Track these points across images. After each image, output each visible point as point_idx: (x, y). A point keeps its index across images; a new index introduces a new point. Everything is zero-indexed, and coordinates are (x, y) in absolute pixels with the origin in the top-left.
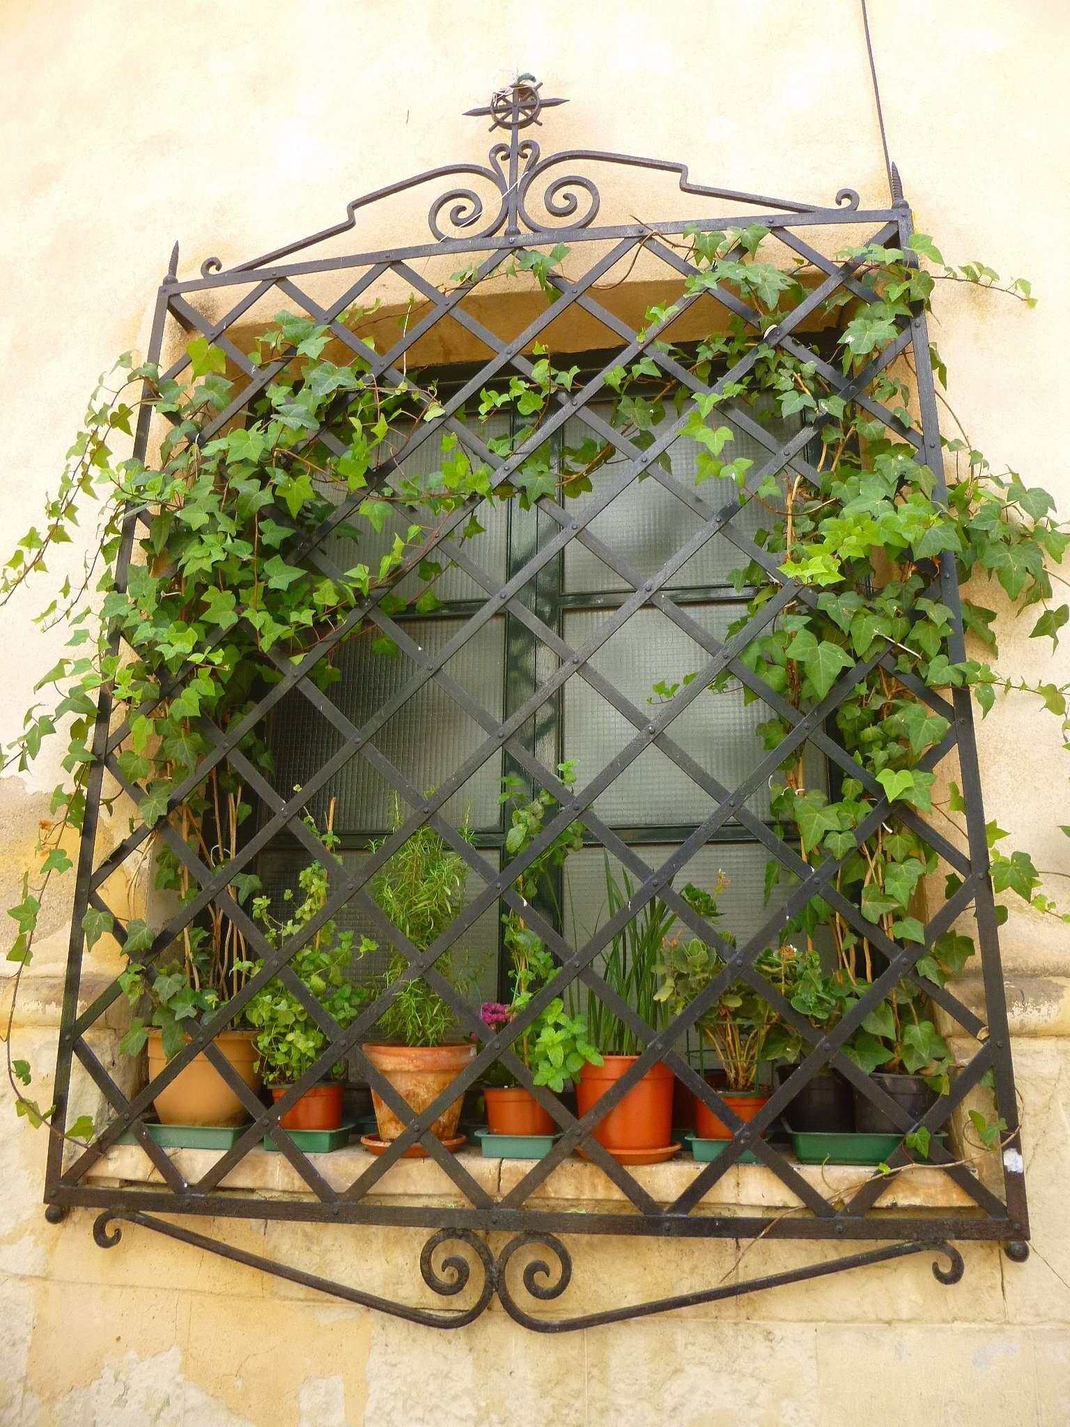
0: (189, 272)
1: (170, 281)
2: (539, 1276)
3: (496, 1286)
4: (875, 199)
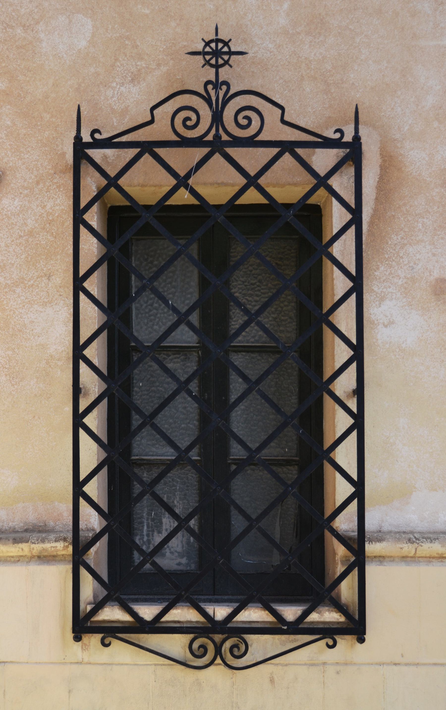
0: (86, 138)
1: (78, 138)
2: (236, 650)
3: (218, 652)
4: (348, 138)
